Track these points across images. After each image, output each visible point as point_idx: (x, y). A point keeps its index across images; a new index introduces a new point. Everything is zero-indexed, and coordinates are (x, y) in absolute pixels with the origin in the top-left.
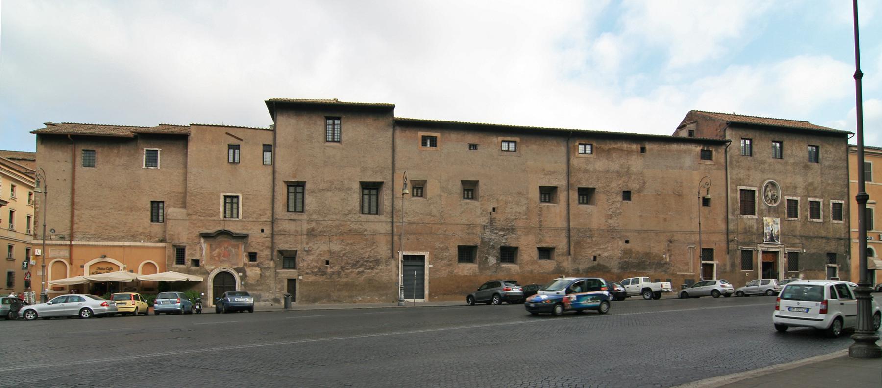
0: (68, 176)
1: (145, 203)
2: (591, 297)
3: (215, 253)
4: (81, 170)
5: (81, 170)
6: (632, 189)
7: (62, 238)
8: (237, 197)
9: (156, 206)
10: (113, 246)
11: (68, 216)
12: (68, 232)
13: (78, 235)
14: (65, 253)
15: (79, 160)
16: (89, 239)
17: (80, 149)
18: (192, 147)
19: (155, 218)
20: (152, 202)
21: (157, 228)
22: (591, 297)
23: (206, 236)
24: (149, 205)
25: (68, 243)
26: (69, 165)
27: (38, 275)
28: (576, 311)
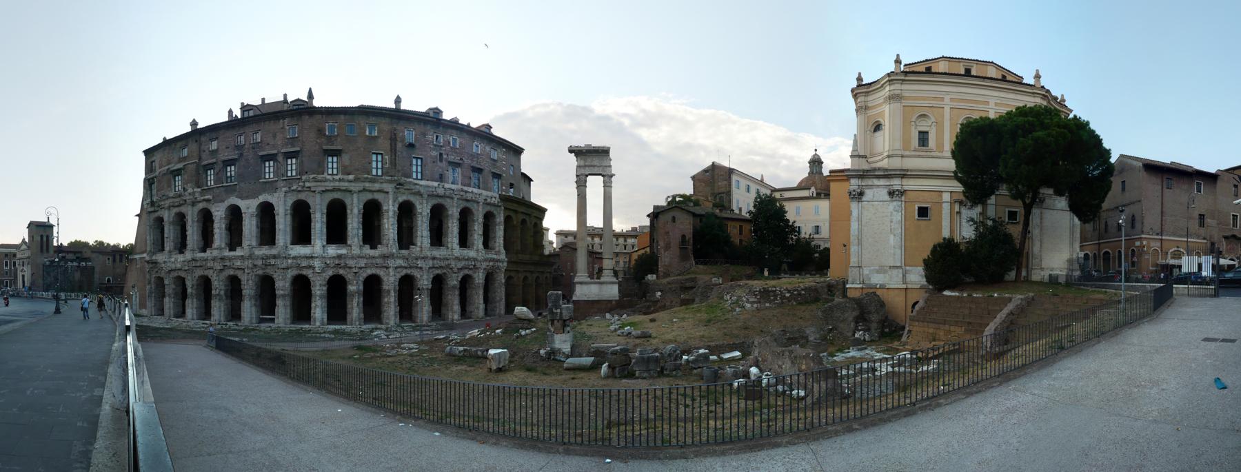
0: (1160, 194)
1: (1196, 215)
2: (1097, 254)
3: (1229, 247)
4: (1166, 191)
5: (1166, 191)
6: (920, 275)
7: (1158, 234)
8: (1237, 216)
9: (1202, 217)
10: (1182, 241)
11: (1160, 220)
12: (1160, 230)
13: (1164, 233)
14: (1158, 244)
15: (1165, 186)
16: (1170, 236)
17: (1166, 176)
18: (1219, 183)
19: (1202, 224)
20: (1200, 215)
21: (1202, 231)
22: (1097, 254)
23: (1226, 238)
24: (1198, 217)
25: (1160, 237)
26: (1160, 187)
27: (827, 236)
28: (681, 199)
